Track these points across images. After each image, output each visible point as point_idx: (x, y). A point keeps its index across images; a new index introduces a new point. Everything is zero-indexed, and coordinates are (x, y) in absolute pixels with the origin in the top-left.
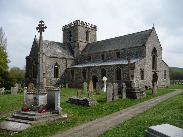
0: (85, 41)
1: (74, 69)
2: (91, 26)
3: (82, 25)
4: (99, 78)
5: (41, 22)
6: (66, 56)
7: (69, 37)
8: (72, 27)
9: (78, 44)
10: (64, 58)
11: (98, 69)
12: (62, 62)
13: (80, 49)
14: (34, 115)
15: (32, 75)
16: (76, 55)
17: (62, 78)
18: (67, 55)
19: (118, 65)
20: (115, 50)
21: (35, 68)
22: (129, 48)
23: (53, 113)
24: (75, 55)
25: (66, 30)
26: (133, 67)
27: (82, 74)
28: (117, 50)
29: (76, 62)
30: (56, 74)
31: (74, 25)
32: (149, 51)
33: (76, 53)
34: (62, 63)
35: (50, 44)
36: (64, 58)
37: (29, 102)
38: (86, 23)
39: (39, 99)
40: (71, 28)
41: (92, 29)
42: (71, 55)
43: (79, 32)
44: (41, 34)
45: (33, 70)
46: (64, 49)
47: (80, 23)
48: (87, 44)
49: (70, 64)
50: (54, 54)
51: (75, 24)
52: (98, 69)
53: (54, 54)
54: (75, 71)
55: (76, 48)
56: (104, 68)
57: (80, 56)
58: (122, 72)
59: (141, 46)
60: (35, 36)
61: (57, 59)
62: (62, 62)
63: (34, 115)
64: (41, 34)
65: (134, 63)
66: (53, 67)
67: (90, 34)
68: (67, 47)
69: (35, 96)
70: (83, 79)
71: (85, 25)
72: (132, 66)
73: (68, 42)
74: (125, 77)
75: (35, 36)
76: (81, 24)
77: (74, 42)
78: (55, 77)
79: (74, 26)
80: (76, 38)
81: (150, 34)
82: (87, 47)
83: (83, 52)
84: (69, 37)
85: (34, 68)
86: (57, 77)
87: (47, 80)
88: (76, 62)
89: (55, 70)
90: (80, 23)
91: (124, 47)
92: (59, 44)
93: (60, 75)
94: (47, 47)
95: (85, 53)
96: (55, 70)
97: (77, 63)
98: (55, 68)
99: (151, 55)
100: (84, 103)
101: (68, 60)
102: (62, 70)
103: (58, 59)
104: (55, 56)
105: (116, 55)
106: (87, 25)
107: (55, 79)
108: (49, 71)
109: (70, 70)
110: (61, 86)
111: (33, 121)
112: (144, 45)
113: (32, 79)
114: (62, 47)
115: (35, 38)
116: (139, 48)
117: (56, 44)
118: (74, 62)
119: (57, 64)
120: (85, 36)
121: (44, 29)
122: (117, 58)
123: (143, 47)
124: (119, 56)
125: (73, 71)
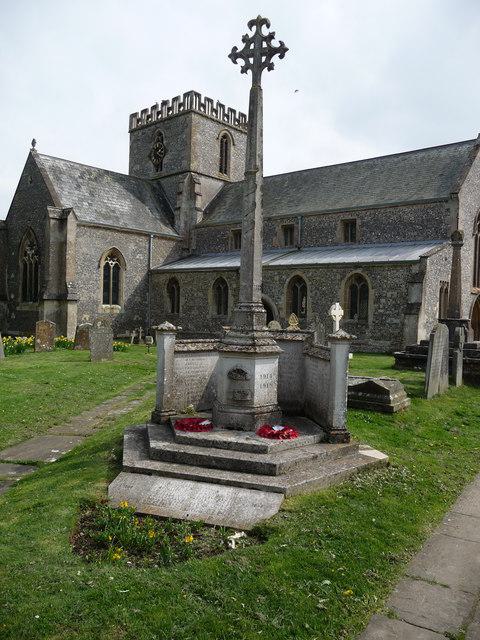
0: (216, 173)
1: (178, 277)
2: (237, 117)
3: (208, 113)
4: (279, 309)
5: (259, 22)
6: (149, 227)
7: (157, 157)
8: (170, 118)
9: (193, 183)
10: (139, 234)
11: (276, 278)
12: (132, 247)
13: (200, 203)
14: (263, 450)
15: (20, 291)
16: (182, 225)
17: (131, 306)
18: (151, 222)
19: (357, 265)
20: (341, 211)
21: (31, 264)
22: (395, 206)
23: (324, 441)
24: (181, 223)
25: (143, 127)
26: (415, 274)
27: (210, 294)
28: (287, 217)
29: (184, 251)
30: (111, 292)
31: (176, 111)
32: (468, 218)
33: (183, 218)
34: (134, 253)
35: (90, 179)
36: (139, 234)
37: (181, 391)
38: (222, 106)
39: (257, 376)
40: (162, 121)
41: (241, 128)
42: (166, 225)
43: (197, 137)
44: (256, 80)
45: (21, 275)
46: (139, 198)
47: (201, 105)
48: (221, 184)
49: (159, 256)
50: (106, 217)
51: (180, 105)
52: (276, 278)
53: (106, 217)
54: (181, 283)
55: (184, 197)
56: (299, 273)
57: (197, 227)
58: (372, 293)
59: (440, 201)
60: (34, 143)
61: (116, 234)
62: (132, 247)
63: (263, 450)
64: (256, 80)
65: (423, 258)
66: (103, 264)
67: (232, 148)
68: (148, 194)
69: (231, 363)
70: (215, 313)
71: (216, 112)
72: (415, 269)
73: (152, 174)
74: (382, 311)
75: (34, 143)
76: (204, 107)
77: (177, 174)
78: (106, 301)
79: (177, 116)
80: (185, 162)
81: (472, 158)
82: (220, 197)
83: (210, 210)
84: (157, 157)
85: (25, 265)
86: (116, 302)
87: (80, 312)
88: (184, 249)
89: (106, 277)
90: (201, 105)
91: (371, 202)
92: (118, 178)
93: (124, 297)
94: (78, 187)
95: (219, 218)
96: (109, 276)
97: (185, 254)
98: (107, 267)
99: (471, 233)
100: (363, 398)
101: (156, 240)
102: (132, 279)
103: (120, 235)
104: (109, 223)
105: (340, 227)
106: (224, 115)
107: (108, 311)
108: (88, 280)
109: (163, 279)
110: (134, 335)
111: (274, 475)
112: (454, 197)
113: (18, 308)
114: (132, 192)
115: (33, 150)
116: (432, 205)
117: (107, 179)
118: (175, 250)
119: (114, 254)
120: (217, 155)
121: (275, 59)
122: (346, 239)
123: (447, 202)
124: (351, 232)
125: (173, 285)
